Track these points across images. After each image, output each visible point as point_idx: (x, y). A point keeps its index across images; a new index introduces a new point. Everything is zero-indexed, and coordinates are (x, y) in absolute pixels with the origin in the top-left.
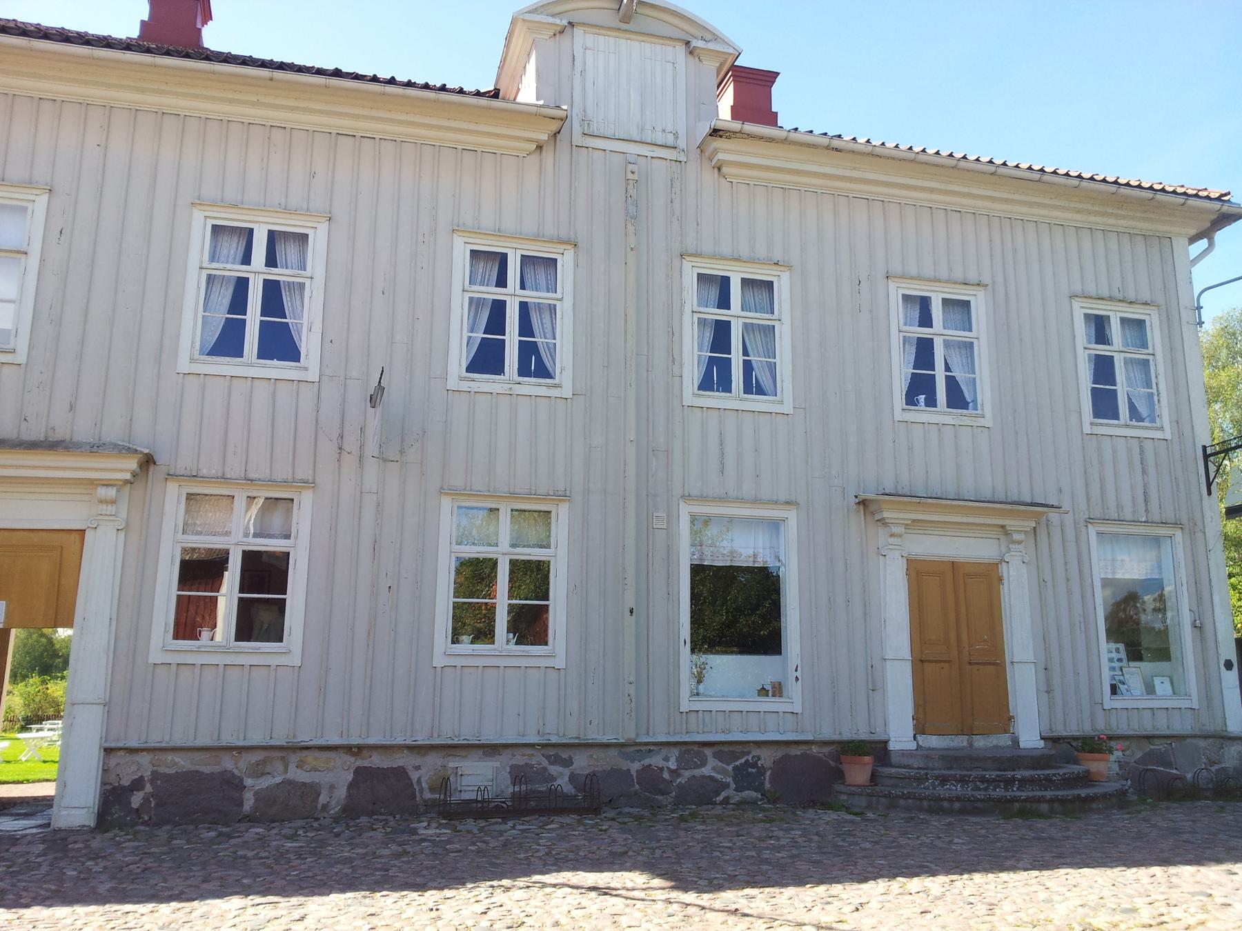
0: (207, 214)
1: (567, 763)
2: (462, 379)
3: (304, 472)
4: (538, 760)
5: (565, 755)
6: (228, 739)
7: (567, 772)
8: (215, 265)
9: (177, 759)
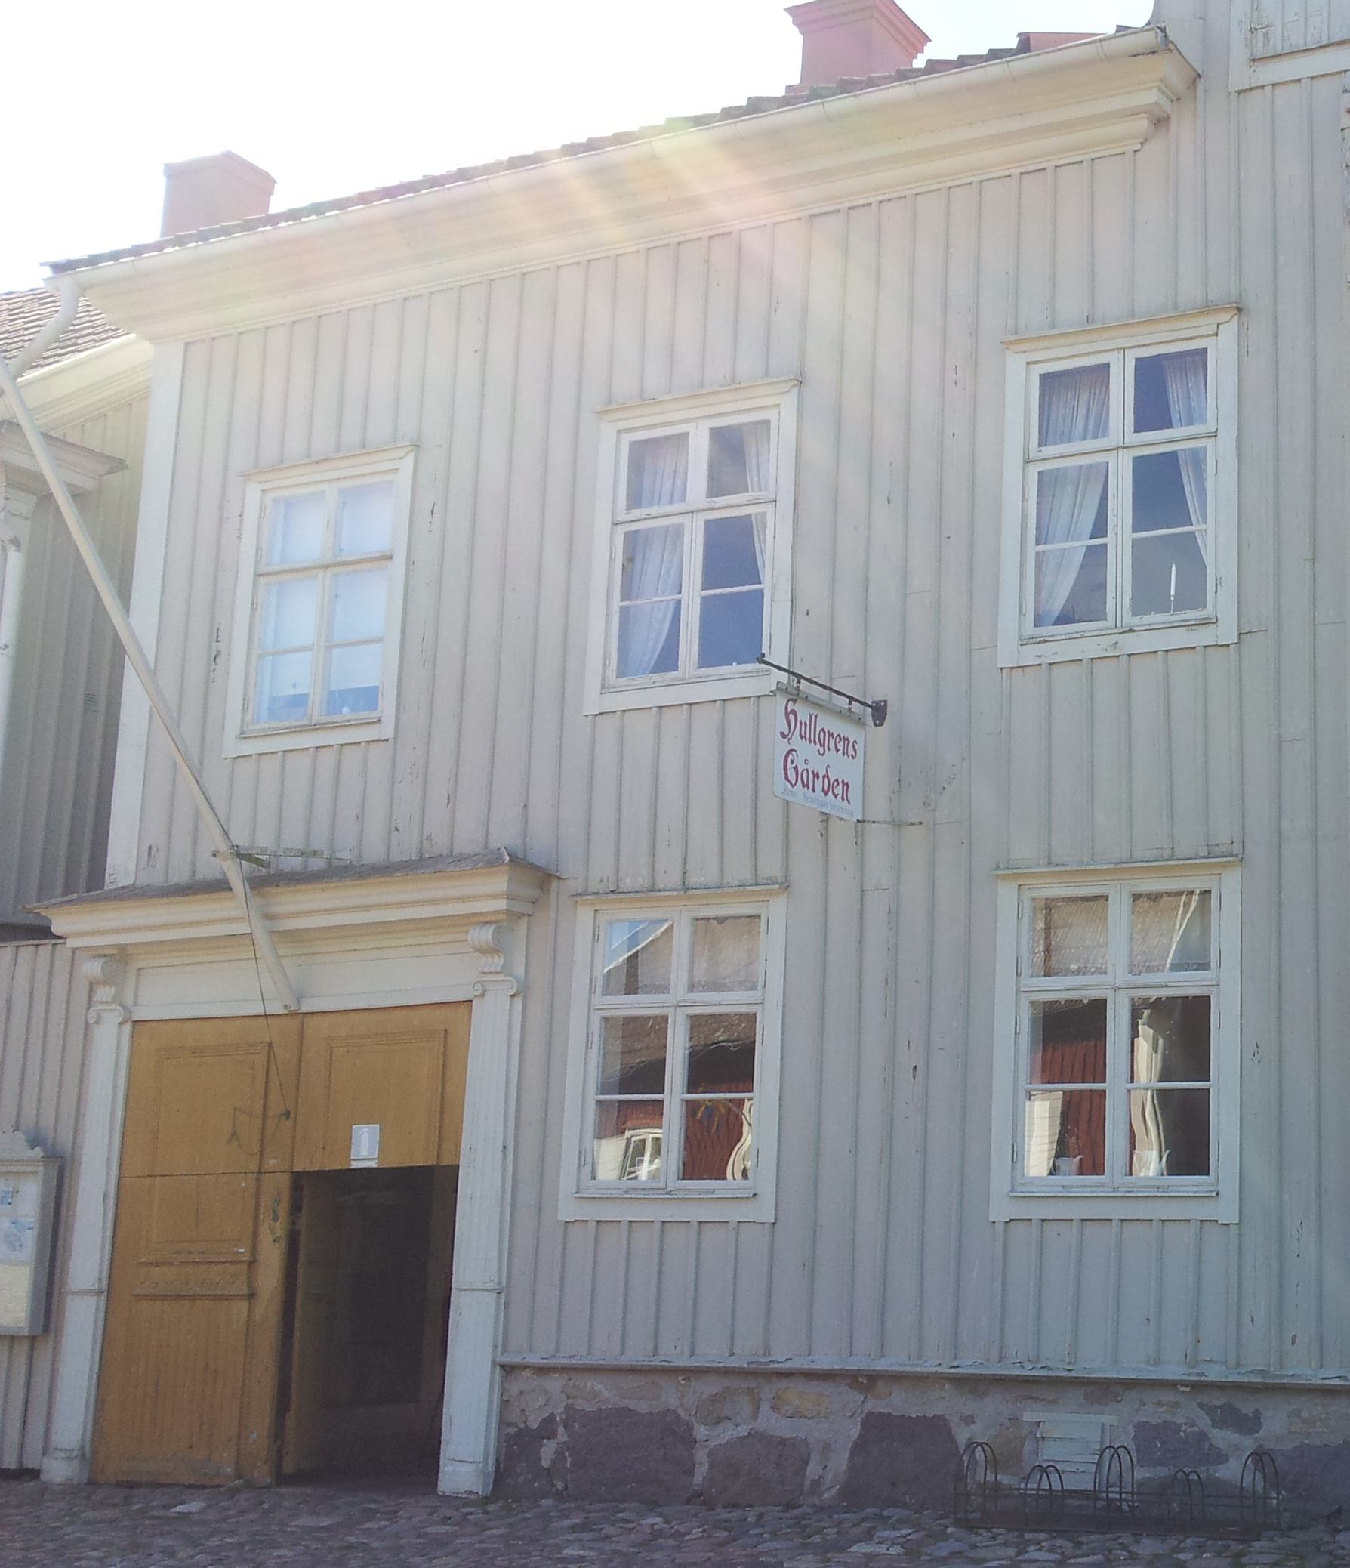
0: (621, 425)
1: (1249, 1424)
2: (1024, 642)
3: (771, 867)
4: (1190, 1416)
5: (1247, 1408)
6: (674, 1354)
7: (1248, 1443)
8: (636, 513)
9: (598, 1387)
